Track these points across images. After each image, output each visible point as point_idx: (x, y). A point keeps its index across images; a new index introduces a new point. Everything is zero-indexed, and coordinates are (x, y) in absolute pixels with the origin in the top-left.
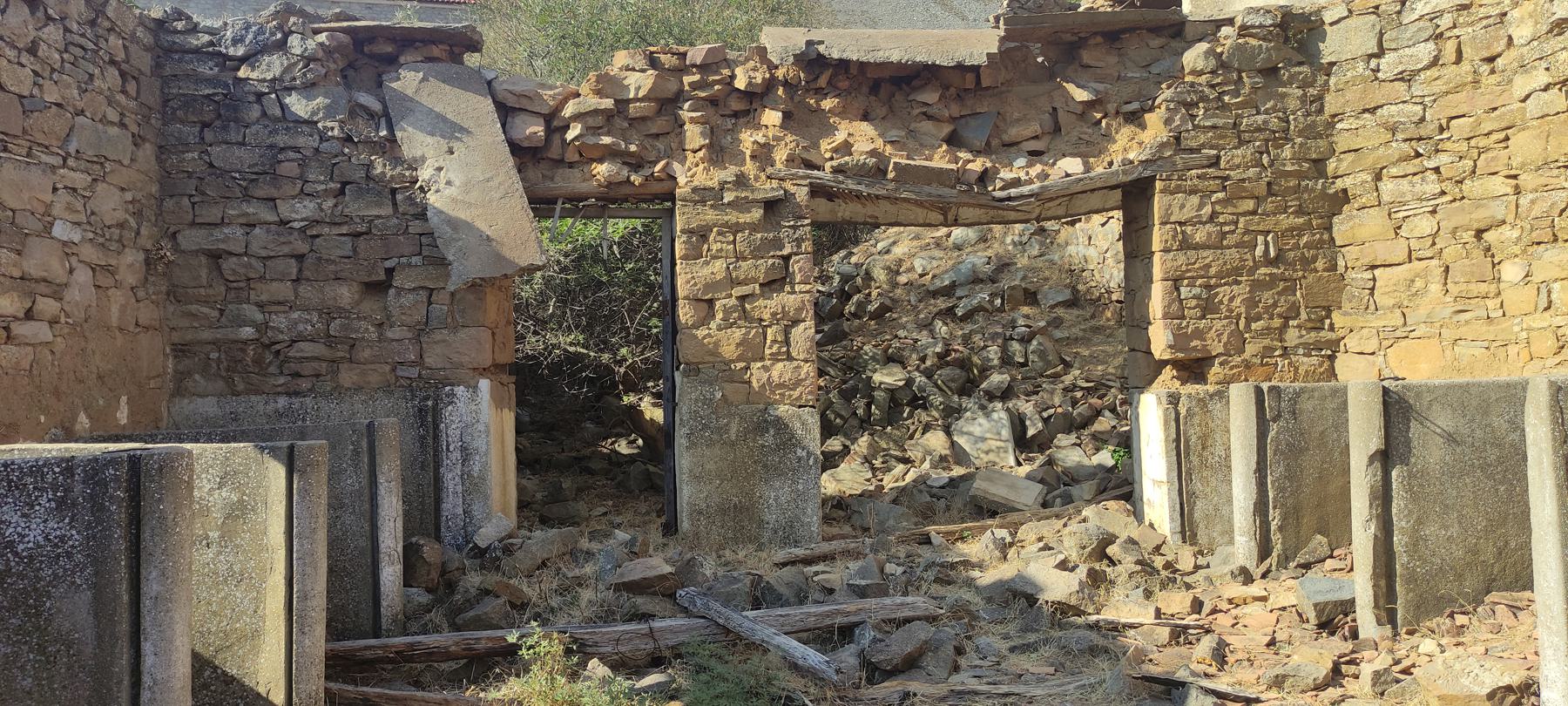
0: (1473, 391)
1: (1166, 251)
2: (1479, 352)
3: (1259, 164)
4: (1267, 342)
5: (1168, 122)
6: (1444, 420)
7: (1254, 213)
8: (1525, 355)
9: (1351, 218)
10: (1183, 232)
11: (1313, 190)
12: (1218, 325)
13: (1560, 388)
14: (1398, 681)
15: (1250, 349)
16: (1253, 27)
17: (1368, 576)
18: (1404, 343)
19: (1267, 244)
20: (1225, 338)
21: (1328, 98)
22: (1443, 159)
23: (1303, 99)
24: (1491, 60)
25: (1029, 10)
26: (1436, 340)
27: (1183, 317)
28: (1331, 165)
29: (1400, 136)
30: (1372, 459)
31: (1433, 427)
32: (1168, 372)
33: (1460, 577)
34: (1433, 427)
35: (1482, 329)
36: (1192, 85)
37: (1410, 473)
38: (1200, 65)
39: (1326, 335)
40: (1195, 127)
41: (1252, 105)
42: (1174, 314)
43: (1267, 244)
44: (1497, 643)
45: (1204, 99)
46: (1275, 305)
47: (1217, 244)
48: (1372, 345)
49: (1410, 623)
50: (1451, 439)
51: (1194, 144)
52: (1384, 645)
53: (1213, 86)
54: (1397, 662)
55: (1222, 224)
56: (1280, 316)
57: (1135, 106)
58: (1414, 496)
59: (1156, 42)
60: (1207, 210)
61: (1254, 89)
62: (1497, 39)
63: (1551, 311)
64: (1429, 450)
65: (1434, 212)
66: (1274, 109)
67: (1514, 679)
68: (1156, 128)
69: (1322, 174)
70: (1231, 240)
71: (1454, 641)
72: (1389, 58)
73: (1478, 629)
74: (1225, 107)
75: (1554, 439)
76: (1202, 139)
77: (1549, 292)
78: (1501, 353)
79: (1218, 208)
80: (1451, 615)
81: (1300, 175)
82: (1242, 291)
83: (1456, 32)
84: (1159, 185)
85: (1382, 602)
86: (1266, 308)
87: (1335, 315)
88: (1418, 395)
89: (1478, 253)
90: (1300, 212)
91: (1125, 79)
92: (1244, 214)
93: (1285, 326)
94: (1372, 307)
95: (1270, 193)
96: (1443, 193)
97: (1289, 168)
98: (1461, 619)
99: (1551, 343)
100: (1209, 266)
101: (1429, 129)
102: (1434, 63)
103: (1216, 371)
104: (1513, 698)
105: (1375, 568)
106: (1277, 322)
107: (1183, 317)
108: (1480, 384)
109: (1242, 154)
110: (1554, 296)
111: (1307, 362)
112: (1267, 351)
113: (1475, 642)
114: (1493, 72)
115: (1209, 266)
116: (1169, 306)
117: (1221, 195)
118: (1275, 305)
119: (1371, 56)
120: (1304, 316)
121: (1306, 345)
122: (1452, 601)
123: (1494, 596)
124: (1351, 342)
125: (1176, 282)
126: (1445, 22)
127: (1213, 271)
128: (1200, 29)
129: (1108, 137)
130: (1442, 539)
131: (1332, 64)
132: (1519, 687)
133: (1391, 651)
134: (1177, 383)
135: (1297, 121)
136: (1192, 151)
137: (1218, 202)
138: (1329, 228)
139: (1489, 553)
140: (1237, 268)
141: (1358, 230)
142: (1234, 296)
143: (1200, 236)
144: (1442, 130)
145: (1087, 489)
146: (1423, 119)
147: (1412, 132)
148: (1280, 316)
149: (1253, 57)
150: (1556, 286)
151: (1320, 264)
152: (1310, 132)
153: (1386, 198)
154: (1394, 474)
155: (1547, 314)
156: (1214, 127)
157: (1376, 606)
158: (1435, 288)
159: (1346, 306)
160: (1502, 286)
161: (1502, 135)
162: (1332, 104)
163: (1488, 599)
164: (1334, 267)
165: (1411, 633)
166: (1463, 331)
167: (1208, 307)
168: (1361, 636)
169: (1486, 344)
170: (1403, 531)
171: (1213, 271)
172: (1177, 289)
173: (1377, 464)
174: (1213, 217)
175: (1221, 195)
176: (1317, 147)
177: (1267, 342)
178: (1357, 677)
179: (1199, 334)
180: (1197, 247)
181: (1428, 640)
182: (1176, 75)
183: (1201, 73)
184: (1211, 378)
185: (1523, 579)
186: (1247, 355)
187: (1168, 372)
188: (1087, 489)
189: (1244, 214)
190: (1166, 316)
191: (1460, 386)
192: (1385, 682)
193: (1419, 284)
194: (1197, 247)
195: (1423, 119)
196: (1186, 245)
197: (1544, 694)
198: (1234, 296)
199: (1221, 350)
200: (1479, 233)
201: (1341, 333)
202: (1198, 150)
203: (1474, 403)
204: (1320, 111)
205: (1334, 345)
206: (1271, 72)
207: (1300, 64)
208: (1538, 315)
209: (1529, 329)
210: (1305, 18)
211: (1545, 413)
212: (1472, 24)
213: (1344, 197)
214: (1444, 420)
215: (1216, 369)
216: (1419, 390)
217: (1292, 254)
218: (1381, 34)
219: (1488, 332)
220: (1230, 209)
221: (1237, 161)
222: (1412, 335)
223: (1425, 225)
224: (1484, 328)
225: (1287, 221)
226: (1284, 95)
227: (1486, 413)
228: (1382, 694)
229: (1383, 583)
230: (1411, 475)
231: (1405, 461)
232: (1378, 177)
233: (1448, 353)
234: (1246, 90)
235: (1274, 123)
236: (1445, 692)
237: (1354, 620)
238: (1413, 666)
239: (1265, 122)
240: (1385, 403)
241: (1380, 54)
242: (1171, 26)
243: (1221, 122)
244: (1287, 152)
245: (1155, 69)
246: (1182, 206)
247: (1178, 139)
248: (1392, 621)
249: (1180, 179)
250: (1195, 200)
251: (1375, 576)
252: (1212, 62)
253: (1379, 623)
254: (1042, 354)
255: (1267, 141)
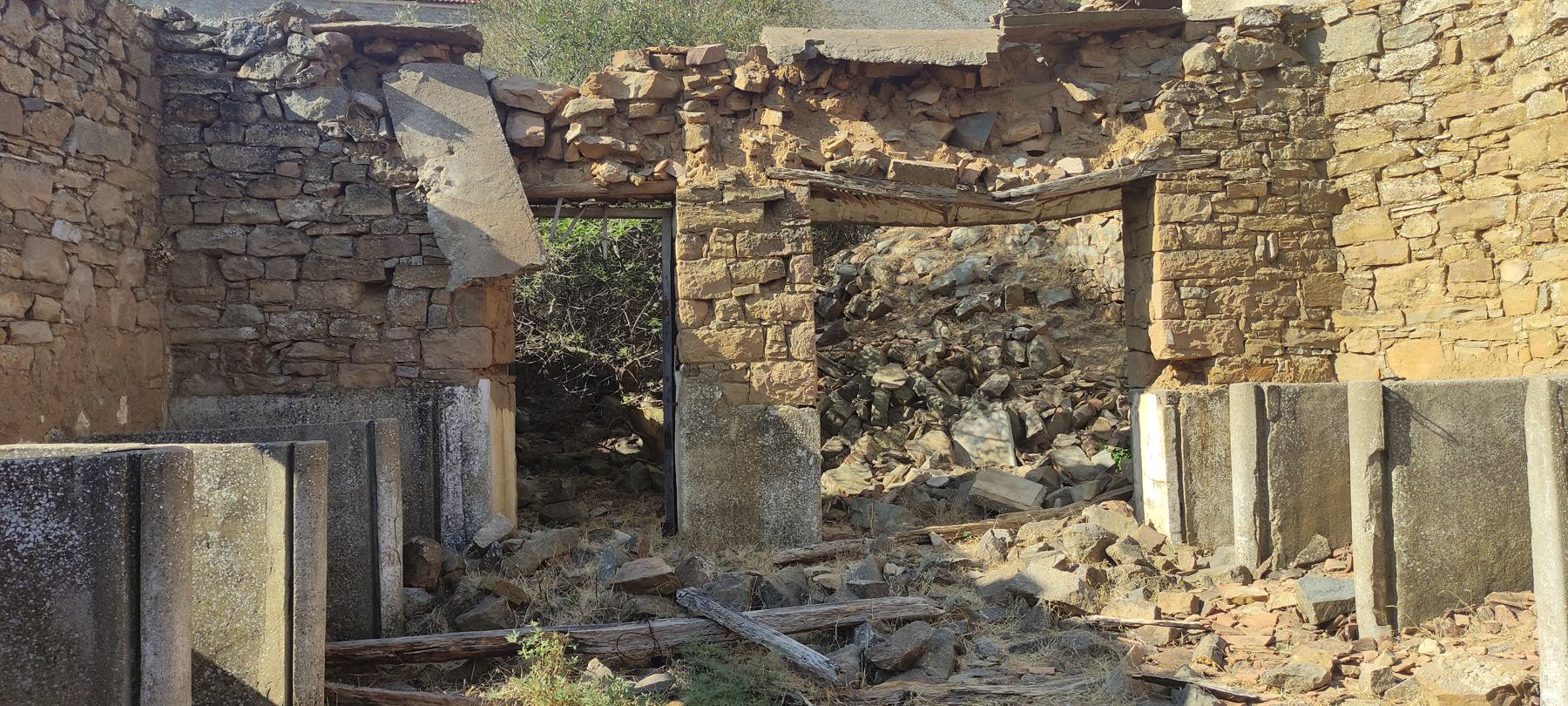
0: (1473, 391)
1: (1166, 251)
2: (1479, 352)
3: (1259, 164)
4: (1267, 342)
5: (1168, 122)
6: (1444, 420)
7: (1254, 213)
8: (1525, 355)
9: (1351, 218)
10: (1183, 232)
11: (1313, 190)
12: (1218, 325)
13: (1560, 388)
14: (1398, 681)
15: (1250, 349)
16: (1253, 27)
17: (1368, 576)
18: (1404, 343)
19: (1267, 244)
20: (1225, 338)
21: (1328, 98)
22: (1443, 159)
23: (1303, 99)
24: (1491, 60)
25: (1029, 10)
26: (1436, 340)
27: (1183, 317)
28: (1331, 165)
29: (1400, 136)
30: (1372, 459)
31: (1433, 427)
32: (1168, 372)
33: (1460, 577)
34: (1433, 427)
35: (1482, 329)
36: (1192, 85)
37: (1410, 473)
38: (1200, 65)
39: (1326, 335)
40: (1195, 127)
41: (1252, 105)
42: (1174, 314)
43: (1267, 244)
44: (1497, 643)
45: (1204, 99)
46: (1275, 305)
47: (1217, 244)
48: (1372, 345)
49: (1410, 623)
50: (1451, 439)
51: (1194, 144)
52: (1384, 645)
53: (1213, 86)
54: (1397, 662)
55: (1222, 224)
56: (1280, 316)
57: (1135, 106)
58: (1414, 496)
59: (1156, 42)
60: (1207, 210)
61: (1254, 89)
62: (1497, 39)
63: (1551, 311)
64: (1429, 450)
65: (1434, 212)
66: (1274, 109)
67: (1514, 679)
68: (1156, 128)
69: (1322, 174)
70: (1231, 240)
71: (1454, 641)
72: (1389, 58)
73: (1478, 629)
74: (1225, 107)
75: (1554, 439)
76: (1202, 139)
77: (1549, 292)
78: (1501, 353)
79: (1218, 208)
80: (1451, 615)
81: (1300, 175)
82: (1242, 291)
83: (1456, 32)
84: (1159, 185)
85: (1382, 602)
86: (1266, 308)
87: (1335, 315)
88: (1418, 395)
89: (1478, 253)
90: (1300, 212)
91: (1125, 79)
92: (1244, 214)
93: (1285, 326)
94: (1372, 307)
95: (1270, 193)
96: (1443, 193)
97: (1289, 168)
98: (1461, 619)
99: (1551, 343)
100: (1209, 266)
101: (1429, 129)
102: (1434, 63)
103: (1216, 371)
104: (1513, 698)
105: (1375, 568)
106: (1277, 322)
107: (1183, 317)
108: (1480, 384)
109: (1242, 154)
110: (1554, 296)
111: (1307, 362)
112: (1267, 351)
113: (1475, 642)
114: (1493, 72)
115: (1209, 266)
116: (1169, 306)
117: (1221, 195)
118: (1275, 305)
119: (1371, 56)
120: (1304, 316)
121: (1306, 345)
122: (1452, 601)
123: (1494, 596)
124: (1351, 342)
125: (1176, 282)
126: (1445, 22)
127: (1213, 271)
128: (1200, 29)
129: (1108, 137)
130: (1442, 539)
131: (1332, 64)
132: (1519, 687)
133: (1391, 651)
134: (1177, 383)
135: (1297, 121)
136: (1192, 151)
137: (1218, 202)
138: (1329, 228)
139: (1489, 553)
140: (1237, 268)
141: (1358, 230)
142: (1234, 296)
143: (1200, 236)
144: (1442, 130)
145: (1087, 489)
146: (1423, 119)
147: (1412, 132)
148: (1280, 316)
149: (1253, 57)
150: (1556, 286)
151: (1320, 264)
152: (1310, 132)
153: (1386, 198)
154: (1394, 474)
155: (1547, 314)
156: (1214, 127)
157: (1376, 606)
158: (1435, 288)
159: (1346, 306)
160: (1502, 286)
161: (1502, 135)
162: (1332, 104)
163: (1488, 599)
164: (1334, 267)
165: (1411, 633)
166: (1463, 331)
167: (1208, 307)
168: (1361, 636)
169: (1486, 344)
170: (1403, 531)
171: (1213, 271)
172: (1177, 289)
173: (1377, 464)
174: (1213, 217)
175: (1221, 195)
176: (1317, 147)
177: (1267, 342)
178: (1357, 677)
179: (1199, 334)
180: (1197, 247)
181: (1428, 640)
182: (1176, 75)
183: (1201, 73)
184: (1211, 378)
185: (1523, 579)
186: (1247, 355)
187: (1168, 372)
188: (1087, 489)
189: (1244, 214)
190: (1166, 316)
191: (1460, 386)
192: (1385, 682)
193: (1419, 284)
194: (1197, 247)
195: (1423, 119)
196: (1186, 245)
197: (1544, 694)
198: (1234, 296)
199: (1221, 350)
200: (1479, 233)
201: (1341, 333)
202: (1198, 150)
203: (1474, 403)
204: (1320, 111)
205: (1334, 345)
206: (1271, 72)
207: (1300, 64)
208: (1538, 315)
209: (1529, 329)
210: (1305, 18)
211: (1545, 413)
212: (1472, 24)
213: (1344, 197)
214: (1444, 420)
215: (1216, 369)
216: (1419, 390)
217: (1292, 254)
218: (1381, 34)
219: (1488, 332)
220: (1230, 209)
221: (1237, 161)
222: (1412, 335)
223: (1425, 225)
224: (1484, 328)
225: (1287, 221)
226: (1284, 95)
227: (1486, 413)
228: (1382, 694)
229: (1383, 583)
230: (1411, 475)
231: (1405, 461)
232: (1378, 177)
233: (1448, 353)
234: (1246, 90)
235: (1274, 123)
236: (1445, 692)
237: (1354, 620)
238: (1413, 666)
239: (1265, 122)
240: (1385, 403)
241: (1380, 54)
242: (1171, 26)
243: (1221, 122)
244: (1287, 152)
245: (1155, 69)
246: (1182, 206)
247: (1178, 139)
248: (1392, 621)
249: (1180, 179)
250: (1195, 200)
251: (1375, 576)
252: (1212, 62)
253: (1379, 623)
254: (1042, 354)
255: (1267, 141)
